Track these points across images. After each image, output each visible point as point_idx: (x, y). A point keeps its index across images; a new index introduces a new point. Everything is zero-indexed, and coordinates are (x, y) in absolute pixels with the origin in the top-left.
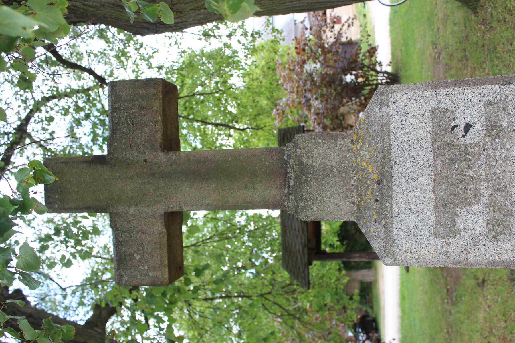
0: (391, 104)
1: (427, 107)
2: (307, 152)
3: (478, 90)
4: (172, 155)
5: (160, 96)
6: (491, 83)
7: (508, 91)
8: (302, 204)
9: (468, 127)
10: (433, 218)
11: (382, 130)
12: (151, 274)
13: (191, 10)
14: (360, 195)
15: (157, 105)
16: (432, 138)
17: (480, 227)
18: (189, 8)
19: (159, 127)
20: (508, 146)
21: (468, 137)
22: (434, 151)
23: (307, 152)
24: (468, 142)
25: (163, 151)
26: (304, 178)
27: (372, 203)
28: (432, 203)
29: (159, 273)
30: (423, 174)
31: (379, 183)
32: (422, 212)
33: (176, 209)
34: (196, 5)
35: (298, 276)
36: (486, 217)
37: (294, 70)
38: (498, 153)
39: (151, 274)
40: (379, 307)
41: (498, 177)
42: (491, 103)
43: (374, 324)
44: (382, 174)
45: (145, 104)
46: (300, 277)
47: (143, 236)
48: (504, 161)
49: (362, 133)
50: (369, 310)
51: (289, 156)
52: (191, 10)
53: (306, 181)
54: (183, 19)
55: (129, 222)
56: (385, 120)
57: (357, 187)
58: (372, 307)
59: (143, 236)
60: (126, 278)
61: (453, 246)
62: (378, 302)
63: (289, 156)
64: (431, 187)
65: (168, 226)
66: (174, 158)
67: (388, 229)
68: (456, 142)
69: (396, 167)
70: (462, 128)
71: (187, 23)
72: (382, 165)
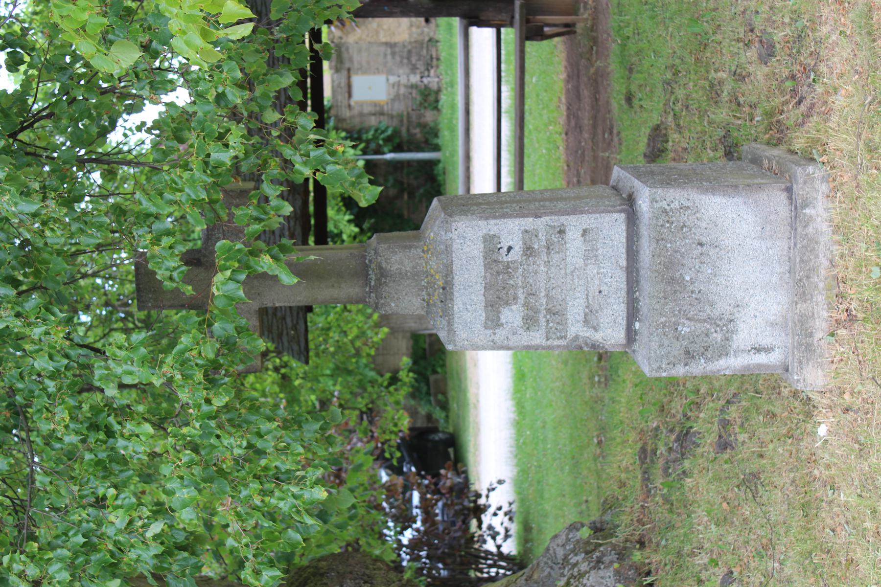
1: (481, 234)
2: (386, 260)
3: (517, 221)
6: (527, 216)
7: (539, 223)
8: (382, 301)
9: (510, 249)
10: (484, 315)
14: (429, 295)
17: (518, 321)
21: (509, 255)
22: (485, 266)
26: (383, 280)
27: (438, 302)
28: (483, 304)
30: (476, 283)
31: (444, 288)
32: (475, 311)
35: (280, 336)
36: (522, 314)
38: (531, 268)
40: (463, 404)
42: (526, 231)
43: (451, 450)
44: (446, 282)
49: (431, 247)
50: (438, 414)
51: (370, 261)
56: (449, 243)
57: (426, 288)
61: (498, 336)
62: (462, 390)
63: (370, 261)
64: (482, 292)
67: (450, 323)
68: (500, 259)
69: (456, 278)
70: (506, 249)
72: (447, 276)
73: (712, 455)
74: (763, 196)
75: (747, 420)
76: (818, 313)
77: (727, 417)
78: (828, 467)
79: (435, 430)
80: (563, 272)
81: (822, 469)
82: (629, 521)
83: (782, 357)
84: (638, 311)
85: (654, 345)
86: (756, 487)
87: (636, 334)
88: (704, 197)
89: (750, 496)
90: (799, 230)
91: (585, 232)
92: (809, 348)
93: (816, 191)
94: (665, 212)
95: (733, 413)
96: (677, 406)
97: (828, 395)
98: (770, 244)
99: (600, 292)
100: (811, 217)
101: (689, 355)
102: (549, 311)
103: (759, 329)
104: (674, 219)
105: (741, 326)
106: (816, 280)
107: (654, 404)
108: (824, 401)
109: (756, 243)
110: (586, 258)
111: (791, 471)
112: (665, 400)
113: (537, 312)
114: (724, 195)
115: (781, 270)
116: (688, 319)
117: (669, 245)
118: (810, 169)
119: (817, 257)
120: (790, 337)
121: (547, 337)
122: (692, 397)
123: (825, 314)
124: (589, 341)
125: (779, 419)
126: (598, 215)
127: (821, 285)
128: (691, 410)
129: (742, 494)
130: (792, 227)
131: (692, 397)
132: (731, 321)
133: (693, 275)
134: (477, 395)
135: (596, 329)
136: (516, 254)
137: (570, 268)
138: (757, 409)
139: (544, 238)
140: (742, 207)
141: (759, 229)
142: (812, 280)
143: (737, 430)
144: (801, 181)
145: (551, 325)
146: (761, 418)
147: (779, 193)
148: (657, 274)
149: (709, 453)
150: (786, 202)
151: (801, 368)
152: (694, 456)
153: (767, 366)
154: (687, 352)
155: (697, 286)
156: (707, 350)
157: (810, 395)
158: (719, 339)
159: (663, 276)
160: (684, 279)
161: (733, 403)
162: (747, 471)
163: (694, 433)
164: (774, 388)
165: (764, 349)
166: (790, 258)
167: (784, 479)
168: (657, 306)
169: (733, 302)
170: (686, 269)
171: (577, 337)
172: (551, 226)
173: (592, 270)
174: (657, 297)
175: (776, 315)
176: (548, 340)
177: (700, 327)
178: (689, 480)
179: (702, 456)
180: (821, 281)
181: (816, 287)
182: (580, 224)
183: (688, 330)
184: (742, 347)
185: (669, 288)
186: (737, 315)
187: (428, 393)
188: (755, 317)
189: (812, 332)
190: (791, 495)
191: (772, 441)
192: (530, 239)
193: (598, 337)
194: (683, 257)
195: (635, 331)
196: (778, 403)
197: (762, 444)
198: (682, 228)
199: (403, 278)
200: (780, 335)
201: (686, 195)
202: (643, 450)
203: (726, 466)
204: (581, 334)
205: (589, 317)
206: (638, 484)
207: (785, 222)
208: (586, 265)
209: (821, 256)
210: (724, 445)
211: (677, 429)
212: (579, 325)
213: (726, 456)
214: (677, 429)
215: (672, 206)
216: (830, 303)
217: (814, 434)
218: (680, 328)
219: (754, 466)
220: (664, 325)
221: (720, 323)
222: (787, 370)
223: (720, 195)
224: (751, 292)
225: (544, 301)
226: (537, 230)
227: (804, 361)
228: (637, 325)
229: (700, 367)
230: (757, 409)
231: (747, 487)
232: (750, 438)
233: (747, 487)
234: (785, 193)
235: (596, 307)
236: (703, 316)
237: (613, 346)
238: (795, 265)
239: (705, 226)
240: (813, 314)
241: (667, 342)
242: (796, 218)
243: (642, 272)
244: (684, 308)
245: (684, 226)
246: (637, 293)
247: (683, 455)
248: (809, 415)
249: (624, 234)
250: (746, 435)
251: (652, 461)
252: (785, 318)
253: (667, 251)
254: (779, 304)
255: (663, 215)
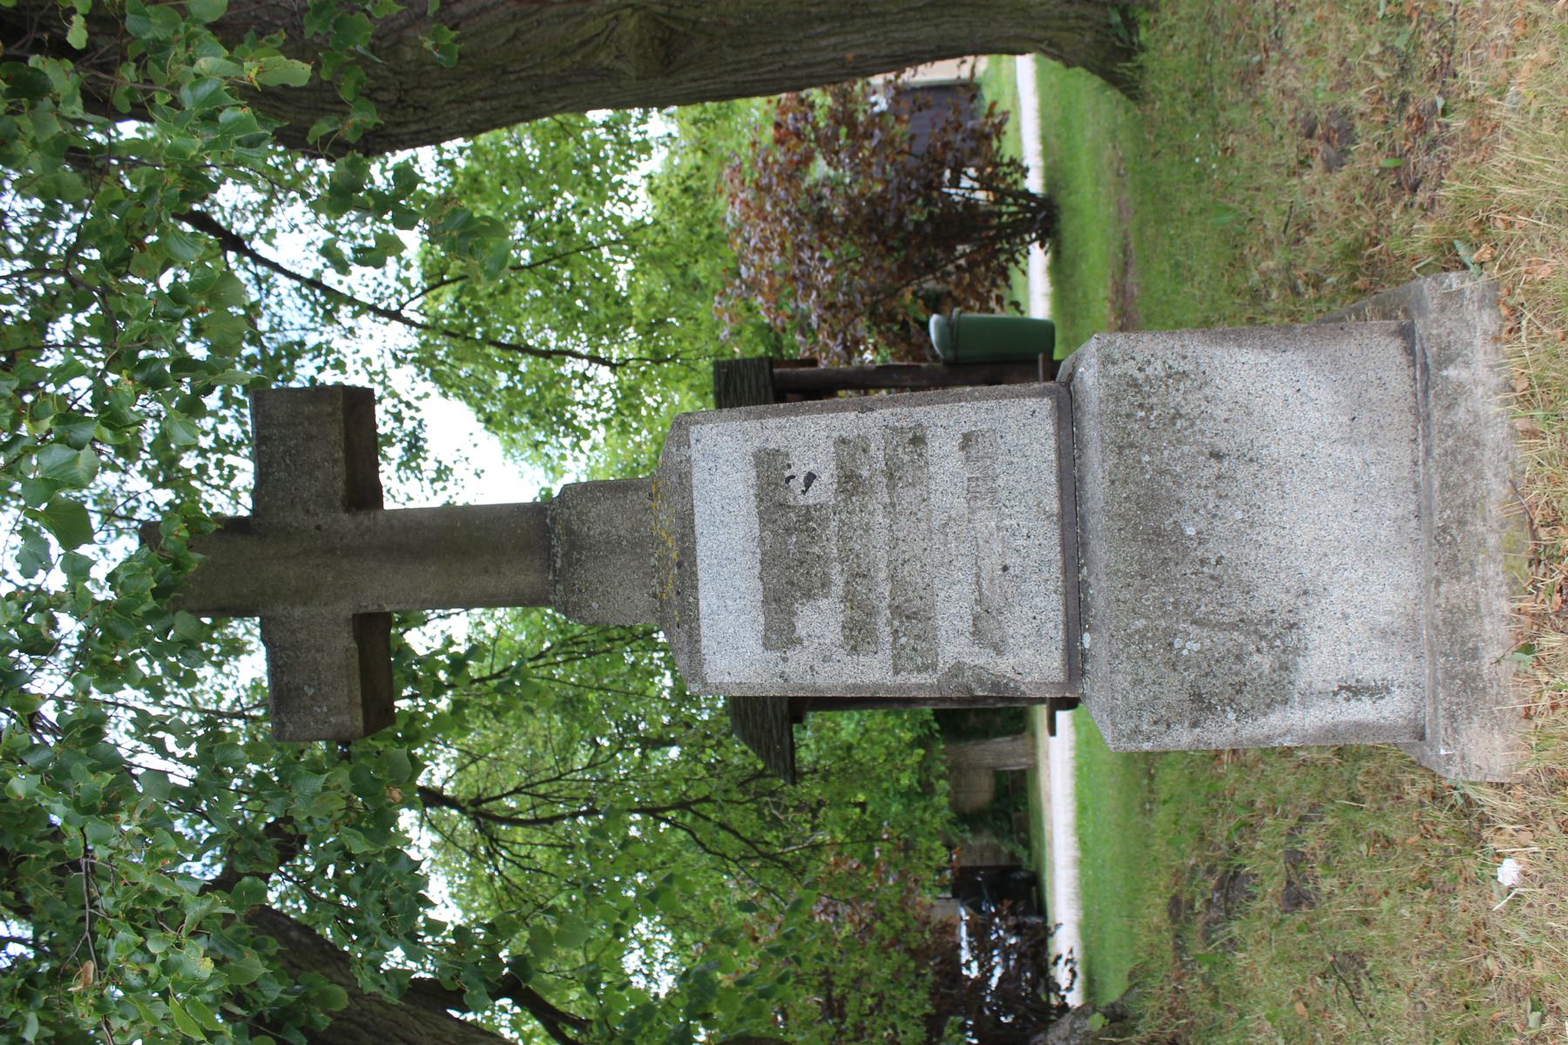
0: (693, 442)
1: (750, 448)
2: (580, 514)
4: (364, 519)
5: (340, 416)
8: (574, 599)
9: (810, 478)
10: (762, 620)
11: (681, 484)
12: (333, 720)
13: (449, 102)
15: (335, 433)
16: (756, 496)
18: (444, 100)
19: (340, 469)
20: (870, 507)
21: (810, 493)
23: (580, 514)
24: (811, 502)
25: (347, 510)
26: (575, 555)
28: (760, 597)
29: (346, 718)
31: (680, 565)
33: (372, 608)
34: (461, 92)
35: (768, 750)
36: (841, 618)
37: (768, 189)
38: (855, 519)
39: (333, 720)
41: (858, 556)
42: (843, 441)
45: (314, 430)
46: (772, 755)
47: (318, 656)
48: (866, 531)
50: (1021, 852)
51: (553, 520)
52: (449, 102)
53: (578, 560)
54: (432, 125)
55: (293, 632)
56: (684, 468)
58: (1027, 845)
59: (318, 656)
60: (290, 727)
61: (792, 664)
62: (1040, 827)
63: (553, 520)
64: (757, 571)
65: (359, 637)
66: (366, 522)
71: (441, 133)
73: (1276, 915)
74: (1348, 347)
75: (1337, 852)
76: (1489, 604)
77: (1298, 847)
78: (1526, 956)
79: (1018, 868)
80: (923, 525)
81: (1506, 959)
82: (1155, 1010)
83: (1408, 707)
84: (1088, 608)
85: (1122, 681)
86: (1357, 979)
87: (1084, 661)
88: (1218, 351)
89: (1346, 996)
90: (1436, 415)
91: (967, 440)
92: (1471, 684)
93: (1470, 327)
94: (1134, 384)
95: (1311, 840)
96: (1222, 830)
97: (1519, 791)
98: (1370, 454)
99: (1005, 569)
100: (1460, 385)
101: (1201, 704)
102: (896, 610)
103: (1355, 645)
104: (1154, 400)
105: (1316, 638)
106: (1481, 529)
107: (1191, 830)
108: (1511, 806)
109: (1340, 452)
110: (972, 496)
111: (1430, 955)
112: (1206, 822)
113: (872, 613)
114: (1263, 347)
115: (1400, 512)
116: (1194, 622)
117: (1146, 458)
118: (1453, 279)
119: (1479, 476)
120: (1425, 663)
121: (895, 665)
122: (1243, 815)
123: (1505, 607)
124: (985, 677)
125: (1399, 850)
126: (992, 403)
127: (1492, 540)
128: (1241, 837)
129: (1330, 989)
130: (1417, 415)
131: (1243, 815)
132: (1292, 626)
133: (1203, 525)
134: (1051, 832)
135: (998, 649)
136: (824, 492)
137: (938, 519)
138: (1356, 831)
139: (881, 454)
140: (1304, 372)
141: (1345, 419)
142: (1469, 528)
143: (1319, 871)
144: (1432, 305)
145: (903, 640)
146: (1363, 847)
147: (1386, 340)
148: (1121, 524)
149: (1271, 911)
150: (1402, 359)
151: (1455, 731)
152: (1247, 915)
153: (1376, 729)
154: (1197, 697)
155: (1213, 550)
156: (1239, 692)
157: (1473, 796)
158: (1266, 668)
159: (1135, 527)
160: (1182, 533)
161: (1311, 820)
162: (1339, 948)
163: (1248, 874)
164: (1388, 788)
165: (1368, 688)
166: (1417, 486)
167: (1418, 972)
168: (1126, 595)
169: (1293, 583)
170: (1187, 512)
171: (958, 668)
172: (894, 429)
173: (986, 522)
174: (1126, 574)
175: (1391, 612)
176: (896, 673)
177: (1225, 641)
178: (1241, 955)
179: (1261, 915)
180: (1492, 531)
181: (1481, 544)
182: (957, 422)
183: (1197, 647)
184: (1319, 686)
185: (1151, 554)
186: (1304, 614)
187: (1011, 831)
188: (1345, 616)
189: (1476, 649)
190: (1431, 1006)
191: (1386, 893)
192: (852, 456)
193: (1004, 666)
194: (1180, 485)
195: (1084, 654)
196: (1396, 818)
197: (1367, 899)
198: (1173, 419)
199: (612, 552)
200: (1402, 658)
201: (1178, 348)
202: (1175, 902)
203: (1301, 937)
204: (967, 660)
205: (983, 624)
206: (1169, 955)
207: (1403, 405)
208: (973, 512)
209: (1489, 474)
210: (1295, 898)
211: (1220, 869)
212: (963, 640)
213: (1300, 918)
214: (1220, 869)
215: (1149, 370)
216: (1515, 581)
217: (1483, 881)
218: (1178, 643)
219: (1353, 939)
220: (1143, 637)
221: (1267, 631)
222: (1422, 737)
223: (1253, 346)
224: (1334, 560)
225: (885, 589)
226: (865, 438)
227: (1462, 713)
228: (1087, 639)
229: (1228, 730)
230: (1356, 831)
231: (1340, 978)
232: (1343, 887)
233: (1340, 978)
234: (1399, 341)
235: (998, 601)
236: (1229, 615)
237: (1038, 686)
238: (1429, 498)
239: (1225, 415)
240: (1477, 606)
241: (1149, 675)
242: (1426, 392)
243: (1092, 522)
244: (1186, 599)
245: (1178, 415)
246: (1085, 571)
247: (1228, 912)
248: (1473, 840)
249: (1052, 443)
250: (1335, 881)
251: (1188, 920)
252: (1412, 619)
253: (1143, 470)
254: (1397, 587)
255: (1132, 391)
